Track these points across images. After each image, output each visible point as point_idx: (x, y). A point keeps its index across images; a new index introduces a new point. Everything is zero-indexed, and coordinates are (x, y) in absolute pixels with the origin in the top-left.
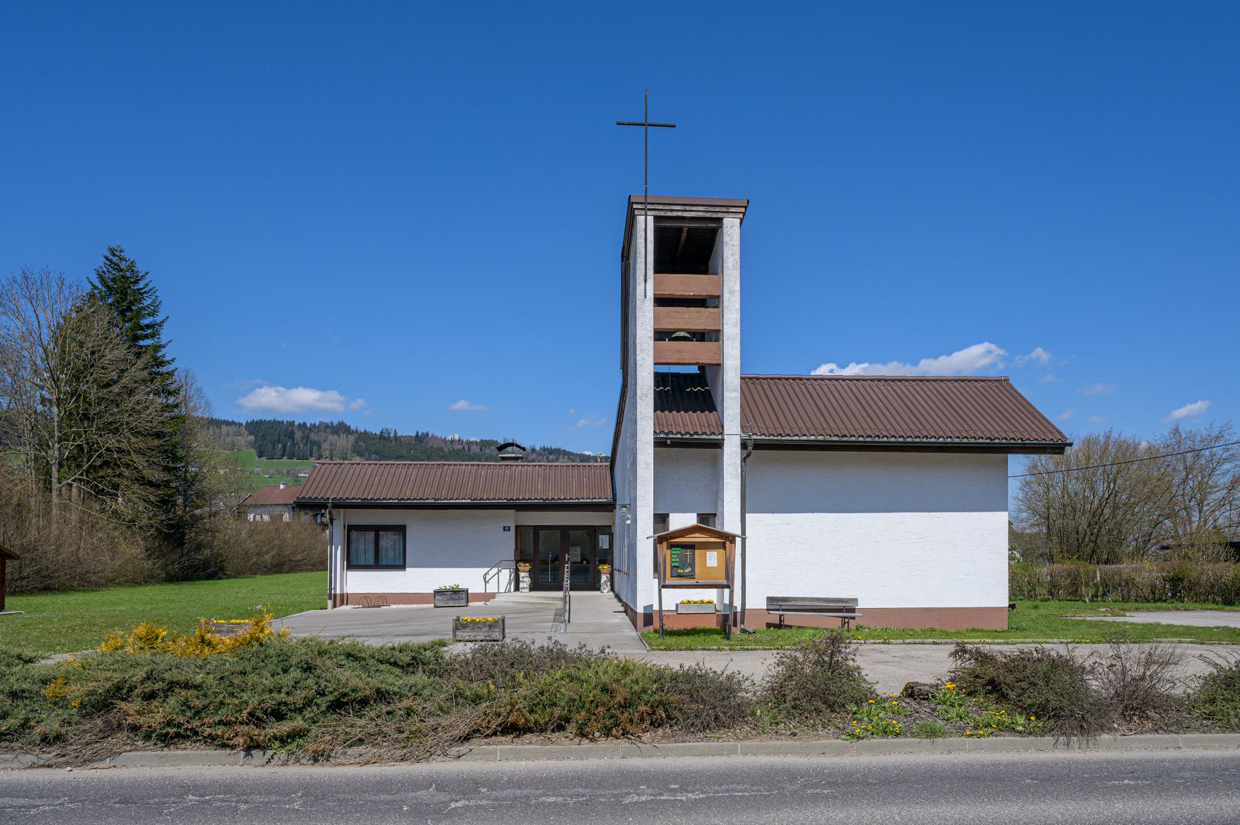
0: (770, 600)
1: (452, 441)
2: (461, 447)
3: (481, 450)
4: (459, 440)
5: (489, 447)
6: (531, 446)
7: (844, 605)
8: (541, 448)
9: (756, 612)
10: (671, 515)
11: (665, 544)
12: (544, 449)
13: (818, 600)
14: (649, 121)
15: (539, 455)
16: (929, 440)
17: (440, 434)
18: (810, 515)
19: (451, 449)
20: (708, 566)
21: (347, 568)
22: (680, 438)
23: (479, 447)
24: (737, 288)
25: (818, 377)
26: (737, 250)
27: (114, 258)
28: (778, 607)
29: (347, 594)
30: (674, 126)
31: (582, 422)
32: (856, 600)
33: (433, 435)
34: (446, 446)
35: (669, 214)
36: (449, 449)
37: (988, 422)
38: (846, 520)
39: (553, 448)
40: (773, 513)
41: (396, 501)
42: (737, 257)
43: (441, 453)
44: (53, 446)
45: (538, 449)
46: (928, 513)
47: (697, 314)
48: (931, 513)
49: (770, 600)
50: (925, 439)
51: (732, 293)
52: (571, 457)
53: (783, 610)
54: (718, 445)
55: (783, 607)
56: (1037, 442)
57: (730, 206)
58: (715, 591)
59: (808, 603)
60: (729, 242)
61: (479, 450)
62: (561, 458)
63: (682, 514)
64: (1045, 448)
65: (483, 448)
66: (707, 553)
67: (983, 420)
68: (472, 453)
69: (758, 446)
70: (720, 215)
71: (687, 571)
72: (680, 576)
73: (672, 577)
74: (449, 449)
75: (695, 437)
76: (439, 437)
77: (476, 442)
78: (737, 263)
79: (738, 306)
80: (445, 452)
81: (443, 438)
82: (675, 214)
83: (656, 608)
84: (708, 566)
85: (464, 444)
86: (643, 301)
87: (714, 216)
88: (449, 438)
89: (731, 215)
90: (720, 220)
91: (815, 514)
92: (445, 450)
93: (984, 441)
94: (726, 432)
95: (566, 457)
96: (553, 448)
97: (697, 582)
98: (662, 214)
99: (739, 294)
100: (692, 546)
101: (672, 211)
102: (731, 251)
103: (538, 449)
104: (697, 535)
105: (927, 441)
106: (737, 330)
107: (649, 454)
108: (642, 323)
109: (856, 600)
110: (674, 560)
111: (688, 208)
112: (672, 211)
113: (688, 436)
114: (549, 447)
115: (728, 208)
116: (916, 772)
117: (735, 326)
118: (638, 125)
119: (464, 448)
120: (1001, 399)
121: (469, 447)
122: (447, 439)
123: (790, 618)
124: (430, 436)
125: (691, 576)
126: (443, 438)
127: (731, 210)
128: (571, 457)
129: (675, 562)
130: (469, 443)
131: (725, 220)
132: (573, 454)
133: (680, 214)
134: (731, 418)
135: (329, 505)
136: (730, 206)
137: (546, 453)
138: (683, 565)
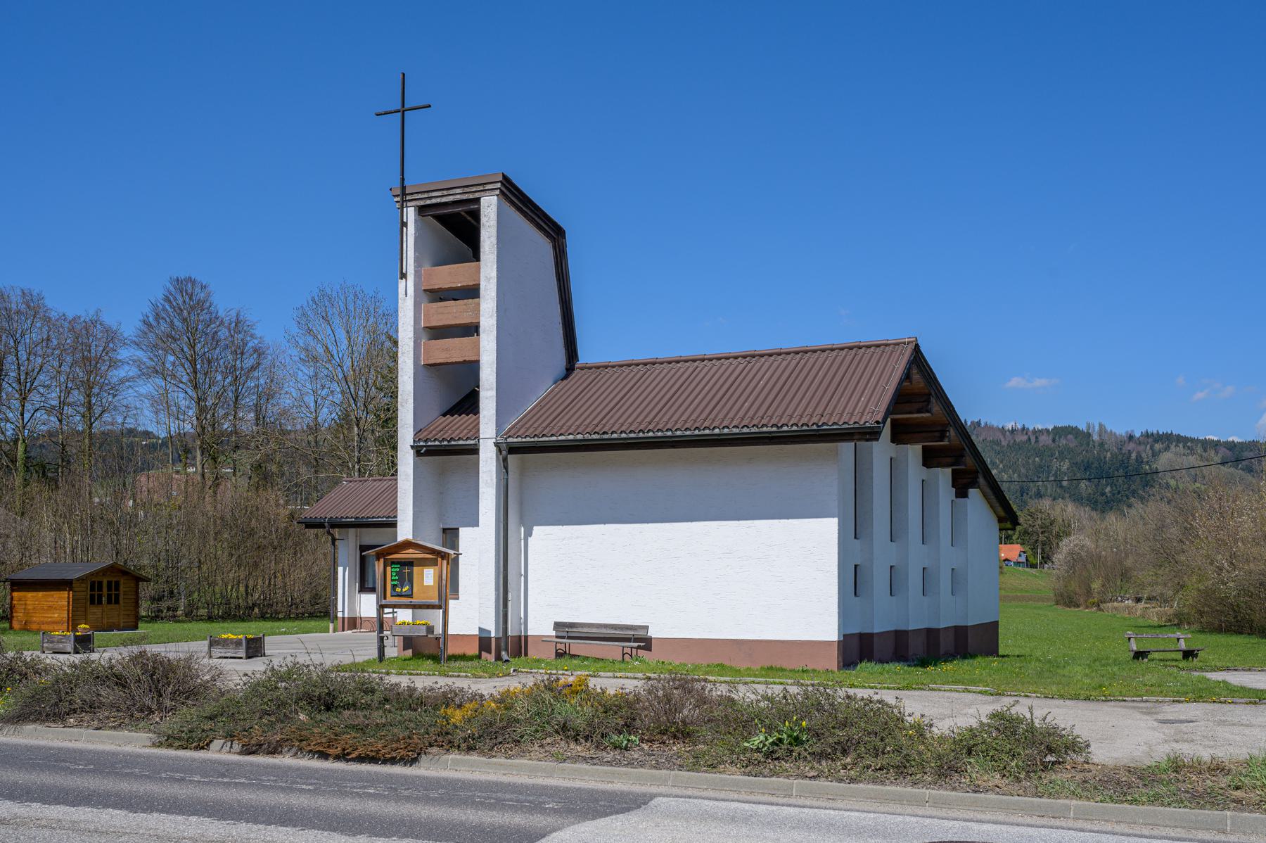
0: (558, 626)
1: (1013, 431)
2: (1025, 438)
3: (1054, 441)
4: (1023, 429)
5: (1066, 437)
6: (1127, 432)
7: (632, 633)
8: (1142, 435)
9: (542, 639)
10: (461, 530)
11: (382, 560)
12: (1147, 435)
13: (606, 626)
14: (399, 107)
15: (1140, 443)
16: (646, 435)
17: (996, 422)
18: (602, 526)
19: (1012, 441)
20: (425, 584)
21: (359, 592)
22: (439, 445)
23: (1051, 436)
24: (494, 274)
25: (664, 360)
26: (494, 231)
27: (184, 285)
28: (565, 634)
29: (361, 618)
30: (430, 106)
31: (1200, 395)
32: (647, 627)
33: (986, 424)
34: (1004, 437)
35: (428, 202)
36: (1009, 442)
37: (582, 415)
38: (641, 532)
39: (1161, 433)
40: (563, 525)
41: (385, 519)
42: (494, 240)
43: (998, 448)
44: (354, 467)
45: (1138, 435)
46: (737, 522)
47: (465, 307)
48: (741, 522)
49: (558, 626)
50: (641, 433)
51: (488, 279)
52: (1189, 444)
53: (569, 638)
54: (474, 451)
55: (570, 635)
56: (838, 427)
57: (485, 184)
58: (410, 611)
59: (594, 630)
60: (485, 223)
61: (1051, 442)
62: (1172, 447)
63: (471, 528)
64: (852, 434)
65: (1057, 438)
66: (425, 570)
67: (639, 410)
68: (1040, 445)
69: (513, 450)
70: (477, 195)
71: (404, 590)
72: (400, 596)
73: (392, 596)
74: (1009, 442)
75: (453, 443)
76: (995, 426)
77: (1047, 430)
78: (493, 246)
79: (494, 294)
80: (1003, 446)
81: (1000, 427)
82: (434, 201)
83: (438, 630)
84: (425, 584)
85: (1029, 434)
86: (404, 300)
87: (471, 196)
88: (1009, 426)
89: (487, 194)
90: (477, 200)
91: (607, 525)
92: (1003, 443)
93: (769, 429)
94: (481, 436)
95: (1181, 445)
96: (1161, 433)
97: (411, 602)
98: (422, 203)
99: (496, 281)
100: (410, 563)
101: (430, 198)
102: (487, 233)
103: (1138, 435)
104: (411, 551)
105: (700, 433)
106: (493, 321)
107: (409, 464)
108: (403, 324)
109: (647, 627)
110: (393, 578)
111: (445, 193)
112: (430, 198)
113: (445, 443)
114: (1155, 432)
115: (483, 186)
116: (522, 810)
117: (491, 316)
118: (384, 114)
119: (1029, 439)
120: (611, 392)
121: (1037, 438)
122: (1007, 428)
123: (577, 647)
124: (983, 425)
125: (410, 596)
126: (1000, 427)
127: (486, 188)
128: (1189, 444)
129: (395, 580)
130: (1037, 433)
131: (482, 199)
132: (1192, 440)
133: (438, 200)
134: (486, 420)
135: (326, 524)
136: (485, 184)
137: (1150, 440)
138: (402, 583)
